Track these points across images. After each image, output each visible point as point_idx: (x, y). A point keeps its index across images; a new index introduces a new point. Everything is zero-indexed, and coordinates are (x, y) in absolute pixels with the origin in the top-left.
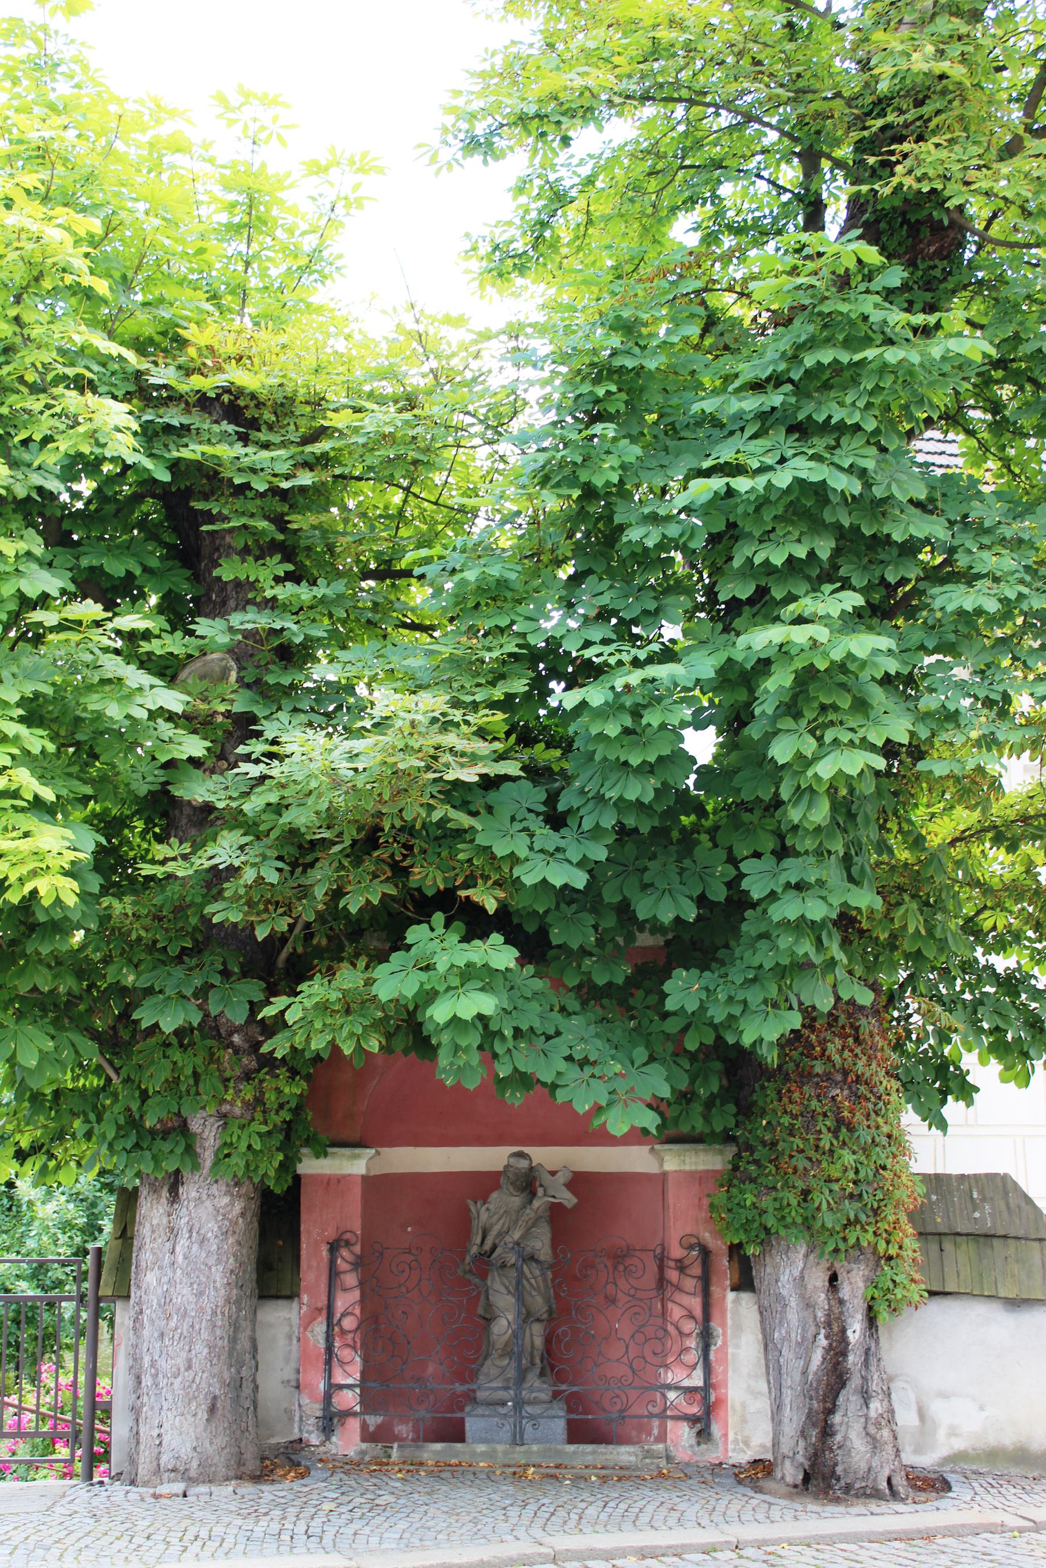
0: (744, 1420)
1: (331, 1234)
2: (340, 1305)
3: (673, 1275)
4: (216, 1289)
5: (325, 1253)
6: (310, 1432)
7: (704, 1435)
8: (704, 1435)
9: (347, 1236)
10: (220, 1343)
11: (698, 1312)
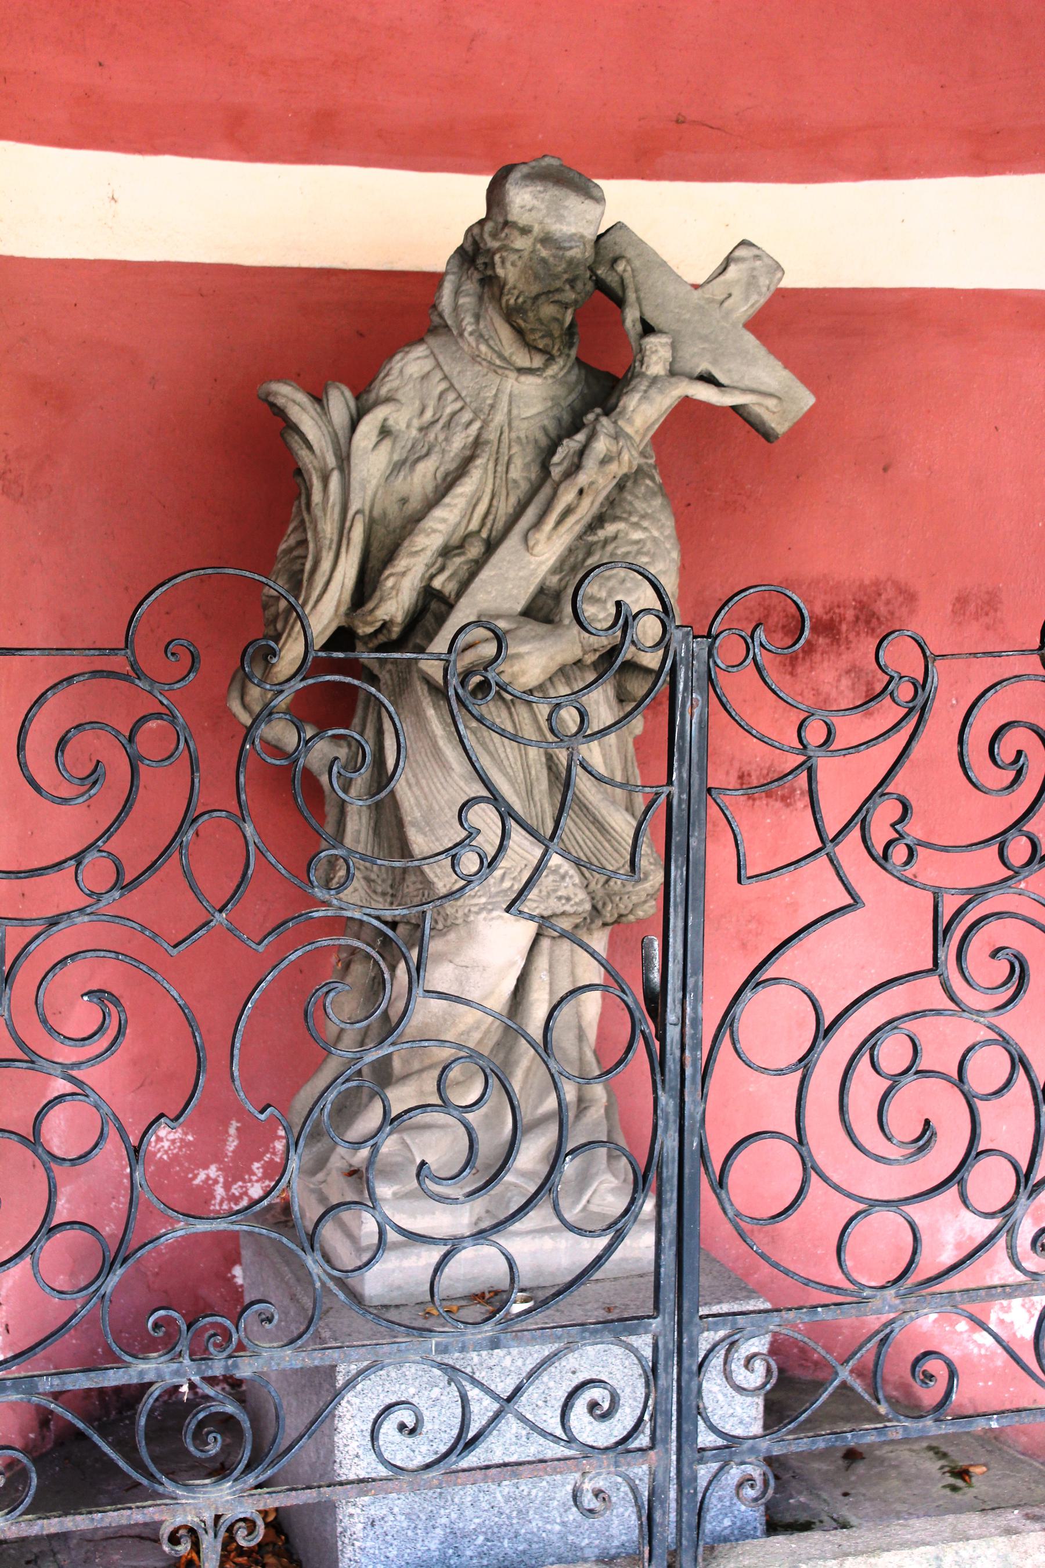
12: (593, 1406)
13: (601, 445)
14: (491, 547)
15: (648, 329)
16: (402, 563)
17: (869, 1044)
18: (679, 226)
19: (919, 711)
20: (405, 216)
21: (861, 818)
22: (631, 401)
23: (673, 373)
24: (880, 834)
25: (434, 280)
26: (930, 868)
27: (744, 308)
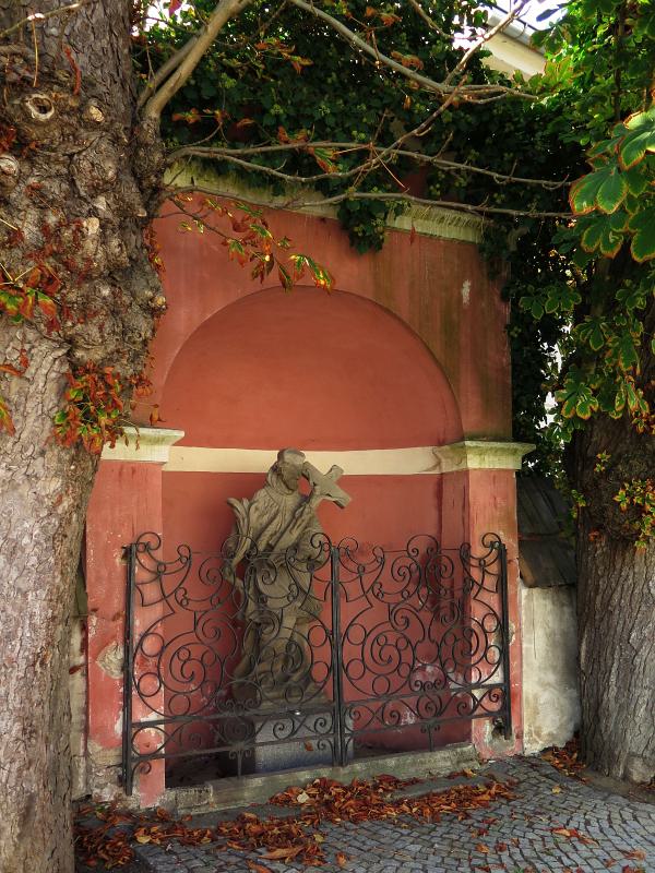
0: (536, 712)
1: (125, 538)
2: (139, 625)
3: (476, 574)
4: (33, 628)
5: (118, 561)
6: (101, 787)
7: (503, 728)
8: (503, 728)
9: (144, 540)
10: (38, 711)
11: (497, 608)
12: (321, 724)
13: (306, 510)
14: (283, 533)
15: (315, 485)
16: (262, 538)
17: (377, 638)
18: (320, 461)
19: (383, 564)
20: (261, 460)
21: (372, 587)
22: (313, 500)
23: (321, 494)
24: (376, 591)
25: (267, 474)
26: (387, 598)
27: (335, 479)
